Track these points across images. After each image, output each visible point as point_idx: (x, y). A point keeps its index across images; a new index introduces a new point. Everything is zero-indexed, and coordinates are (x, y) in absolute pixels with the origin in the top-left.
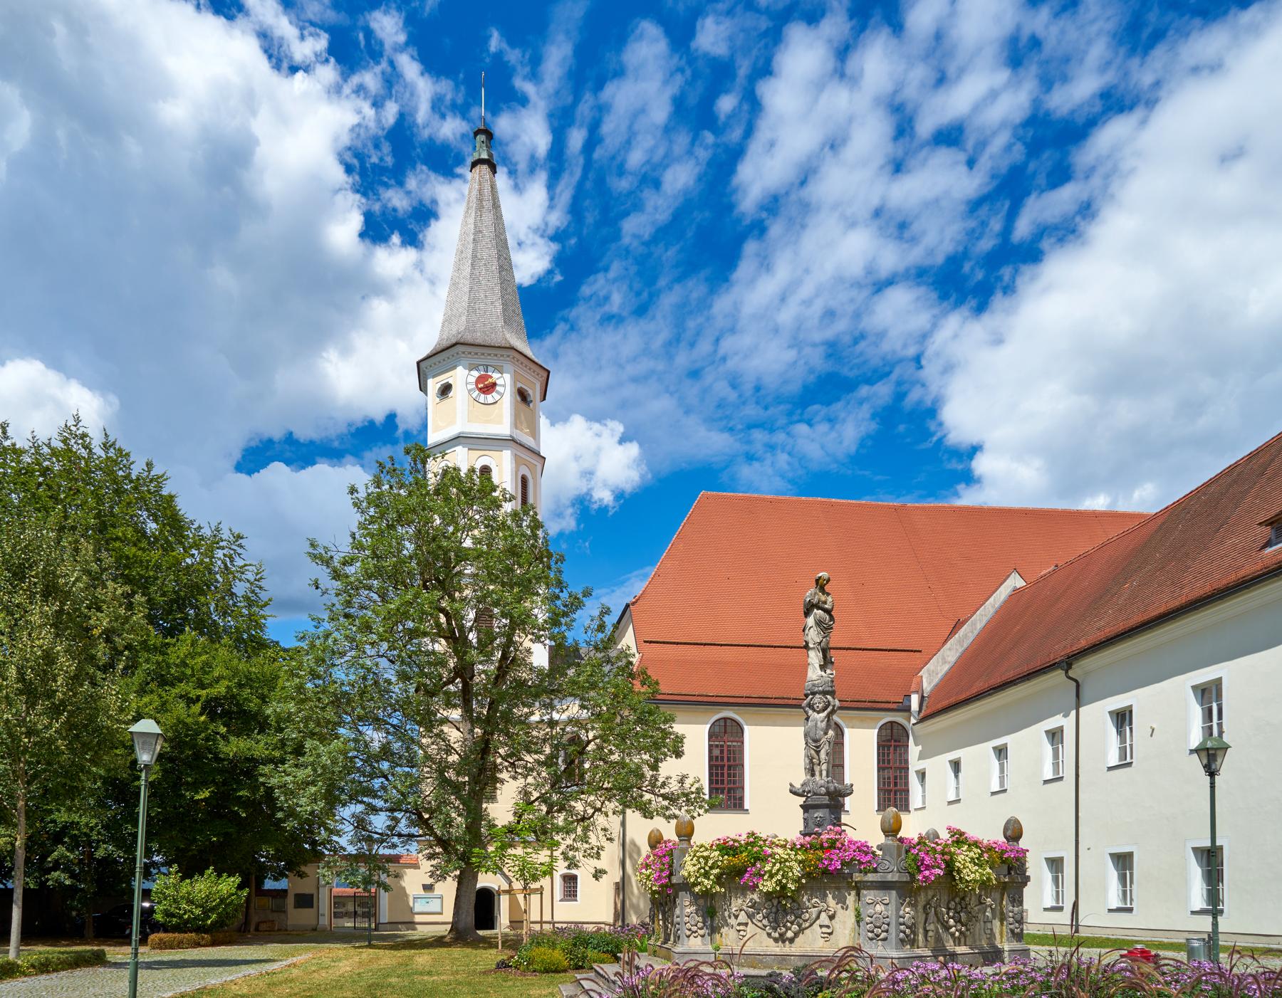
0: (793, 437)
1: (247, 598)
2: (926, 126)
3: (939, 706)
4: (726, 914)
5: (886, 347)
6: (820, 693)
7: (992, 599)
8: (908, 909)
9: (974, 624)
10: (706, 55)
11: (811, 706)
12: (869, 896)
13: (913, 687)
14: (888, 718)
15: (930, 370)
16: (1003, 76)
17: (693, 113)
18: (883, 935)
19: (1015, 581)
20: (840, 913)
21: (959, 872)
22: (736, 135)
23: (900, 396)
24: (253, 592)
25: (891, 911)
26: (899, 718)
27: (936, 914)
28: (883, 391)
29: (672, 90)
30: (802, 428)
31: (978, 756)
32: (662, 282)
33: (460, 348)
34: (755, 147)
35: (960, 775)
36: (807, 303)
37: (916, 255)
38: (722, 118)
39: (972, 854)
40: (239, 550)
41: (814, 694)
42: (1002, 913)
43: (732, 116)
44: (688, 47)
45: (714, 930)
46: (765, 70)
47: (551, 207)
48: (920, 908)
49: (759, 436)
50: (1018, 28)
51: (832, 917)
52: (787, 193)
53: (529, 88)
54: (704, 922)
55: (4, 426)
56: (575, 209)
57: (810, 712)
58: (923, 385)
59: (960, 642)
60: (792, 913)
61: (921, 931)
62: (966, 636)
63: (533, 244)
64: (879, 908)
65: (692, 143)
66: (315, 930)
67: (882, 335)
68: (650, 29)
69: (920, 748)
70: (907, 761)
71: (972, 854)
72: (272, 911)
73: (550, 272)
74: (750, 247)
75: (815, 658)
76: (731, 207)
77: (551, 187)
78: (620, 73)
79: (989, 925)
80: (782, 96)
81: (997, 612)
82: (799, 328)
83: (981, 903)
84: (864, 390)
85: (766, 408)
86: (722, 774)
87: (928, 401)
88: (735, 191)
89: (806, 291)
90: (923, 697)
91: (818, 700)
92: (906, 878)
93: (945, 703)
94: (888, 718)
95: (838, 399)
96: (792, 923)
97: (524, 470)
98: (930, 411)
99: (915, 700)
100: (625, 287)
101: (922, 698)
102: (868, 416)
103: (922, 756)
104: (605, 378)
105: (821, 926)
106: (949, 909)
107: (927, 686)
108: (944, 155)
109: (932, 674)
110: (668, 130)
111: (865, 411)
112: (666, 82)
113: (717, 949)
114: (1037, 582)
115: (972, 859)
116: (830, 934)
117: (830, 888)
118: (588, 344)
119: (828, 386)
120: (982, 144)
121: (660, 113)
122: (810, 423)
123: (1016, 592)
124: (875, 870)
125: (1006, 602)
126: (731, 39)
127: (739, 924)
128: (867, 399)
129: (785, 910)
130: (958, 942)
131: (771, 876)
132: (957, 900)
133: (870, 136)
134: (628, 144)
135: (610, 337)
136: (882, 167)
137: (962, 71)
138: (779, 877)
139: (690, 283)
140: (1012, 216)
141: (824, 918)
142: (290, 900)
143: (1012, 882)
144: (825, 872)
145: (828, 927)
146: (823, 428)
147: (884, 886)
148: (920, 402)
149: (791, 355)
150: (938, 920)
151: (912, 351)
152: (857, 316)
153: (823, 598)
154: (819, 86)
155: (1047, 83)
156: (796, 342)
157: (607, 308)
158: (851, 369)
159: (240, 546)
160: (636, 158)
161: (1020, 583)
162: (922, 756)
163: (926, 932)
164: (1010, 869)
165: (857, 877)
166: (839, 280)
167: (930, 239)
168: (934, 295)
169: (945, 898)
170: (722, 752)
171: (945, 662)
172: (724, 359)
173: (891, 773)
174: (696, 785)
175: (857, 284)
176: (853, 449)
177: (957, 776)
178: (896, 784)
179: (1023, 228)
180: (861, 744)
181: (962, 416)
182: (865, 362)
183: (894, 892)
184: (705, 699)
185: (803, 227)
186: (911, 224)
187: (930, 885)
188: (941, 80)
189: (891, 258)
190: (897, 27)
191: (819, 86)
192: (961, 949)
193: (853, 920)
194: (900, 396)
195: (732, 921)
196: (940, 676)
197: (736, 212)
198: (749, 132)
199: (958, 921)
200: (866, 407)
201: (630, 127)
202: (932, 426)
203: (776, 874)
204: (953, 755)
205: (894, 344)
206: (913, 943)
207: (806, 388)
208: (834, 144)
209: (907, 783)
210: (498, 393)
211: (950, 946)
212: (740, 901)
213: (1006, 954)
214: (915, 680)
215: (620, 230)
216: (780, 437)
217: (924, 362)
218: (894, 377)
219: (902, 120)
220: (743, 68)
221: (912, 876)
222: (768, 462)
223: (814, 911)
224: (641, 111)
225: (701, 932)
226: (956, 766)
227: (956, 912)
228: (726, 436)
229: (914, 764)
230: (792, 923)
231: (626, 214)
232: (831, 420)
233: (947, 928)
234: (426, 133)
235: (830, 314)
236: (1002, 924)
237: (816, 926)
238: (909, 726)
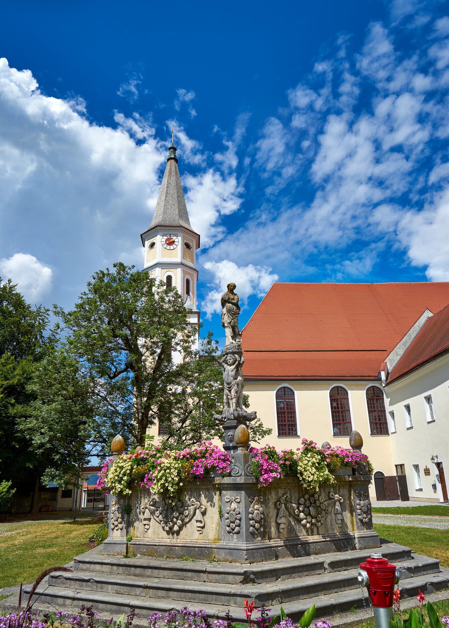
0: (344, 266)
1: (49, 338)
2: (386, 147)
3: (395, 377)
4: (138, 510)
5: (380, 228)
6: (231, 353)
7: (417, 323)
8: (256, 507)
9: (410, 335)
10: (296, 128)
11: (226, 362)
12: (228, 495)
13: (382, 368)
14: (371, 384)
15: (402, 236)
16: (418, 126)
17: (294, 148)
18: (237, 529)
19: (428, 314)
20: (210, 509)
21: (301, 474)
22: (311, 154)
23: (389, 247)
24: (54, 335)
25: (242, 508)
26: (376, 384)
27: (285, 507)
28: (381, 245)
29: (284, 141)
30: (347, 262)
31: (417, 402)
32: (282, 209)
33: (158, 228)
34: (319, 158)
35: (411, 413)
36: (345, 214)
37: (388, 193)
38: (304, 149)
39: (314, 460)
40: (47, 316)
41: (227, 354)
42: (351, 506)
43: (309, 147)
44: (290, 126)
45: (129, 524)
46: (321, 131)
47: (237, 186)
48: (271, 504)
49: (328, 266)
50: (421, 110)
51: (204, 514)
52: (333, 174)
53: (230, 144)
54: (122, 518)
55: (0, 278)
56: (246, 186)
57: (225, 366)
58: (400, 242)
59: (404, 344)
60: (177, 510)
61: (273, 524)
62: (406, 341)
63: (231, 199)
64: (234, 505)
65: (294, 159)
66: (71, 510)
67: (378, 224)
68: (274, 120)
69: (389, 399)
70: (384, 407)
71: (314, 460)
72: (50, 500)
73: (239, 210)
74: (319, 194)
75: (228, 332)
76: (310, 181)
77: (238, 179)
78: (263, 137)
79: (339, 517)
80: (328, 140)
81: (421, 329)
82: (341, 223)
83: (330, 499)
84: (373, 245)
85: (331, 255)
86: (285, 417)
87: (402, 248)
88: (311, 175)
89: (343, 209)
90: (388, 373)
91: (230, 358)
92: (252, 480)
93: (398, 375)
94: (371, 384)
95: (362, 250)
96: (177, 519)
97: (188, 277)
98: (403, 253)
99: (383, 375)
100: (267, 212)
101: (388, 374)
102: (375, 256)
103: (390, 405)
104: (259, 246)
105: (197, 521)
106: (299, 504)
107: (390, 367)
108: (396, 156)
109: (392, 361)
110: (284, 154)
111: (374, 254)
112: (282, 138)
113: (130, 539)
114: (438, 313)
115: (313, 464)
116: (203, 527)
117: (203, 489)
118: (251, 234)
119: (357, 245)
120: (411, 151)
121: (280, 148)
122: (351, 260)
123: (429, 319)
124: (230, 475)
125: (425, 324)
126: (306, 122)
127: (145, 519)
128: (374, 249)
129: (172, 508)
130: (310, 532)
131: (158, 481)
132: (307, 497)
133: (365, 151)
134: (267, 160)
135: (261, 230)
136: (372, 161)
137: (399, 126)
138: (162, 482)
139: (295, 209)
140: (428, 176)
141: (198, 515)
142: (60, 494)
143: (356, 480)
144: (196, 477)
145: (201, 522)
146: (357, 261)
147: (236, 487)
148: (398, 249)
149: (340, 233)
150: (290, 514)
151: (392, 229)
152: (366, 218)
153: (232, 297)
154: (342, 135)
155: (435, 126)
156: (341, 227)
157: (259, 220)
158: (366, 237)
159: (48, 315)
160: (270, 166)
161: (431, 315)
162: (390, 405)
163: (278, 525)
164: (354, 471)
165: (218, 480)
166: (356, 204)
167: (395, 188)
168: (401, 207)
169: (295, 495)
170: (338, 404)
171: (397, 355)
172: (310, 236)
173: (376, 414)
174: (259, 423)
175: (364, 205)
176: (371, 270)
177: (409, 414)
178: (380, 420)
179: (433, 178)
180: (357, 400)
181: (417, 254)
182: (372, 234)
183: (243, 492)
184: (273, 378)
185: (340, 185)
186: (385, 182)
187: (275, 485)
188: (392, 130)
189: (378, 195)
190: (372, 114)
191: (342, 135)
192: (311, 539)
193: (218, 516)
194: (389, 247)
195: (141, 517)
196: (396, 362)
197: (312, 182)
198: (316, 153)
199: (308, 514)
200: (374, 252)
201: (268, 155)
202: (406, 258)
203: (161, 479)
204: (406, 402)
205: (382, 227)
206: (265, 535)
207: (348, 245)
208: (350, 155)
209: (386, 419)
210: (175, 245)
211: (303, 536)
212: (146, 500)
213: (356, 541)
214: (382, 365)
215: (265, 192)
216: (338, 266)
217: (398, 233)
218: (385, 239)
219: (377, 144)
220: (312, 131)
221: (257, 479)
222: (333, 277)
223: (192, 508)
224: (272, 149)
225: (120, 526)
226: (408, 408)
227: (305, 506)
228: (315, 268)
229: (388, 408)
230: (177, 519)
231: (267, 186)
232: (360, 259)
233: (299, 521)
234: (187, 162)
235: (354, 217)
236: (352, 515)
237: (193, 521)
238: (382, 388)
